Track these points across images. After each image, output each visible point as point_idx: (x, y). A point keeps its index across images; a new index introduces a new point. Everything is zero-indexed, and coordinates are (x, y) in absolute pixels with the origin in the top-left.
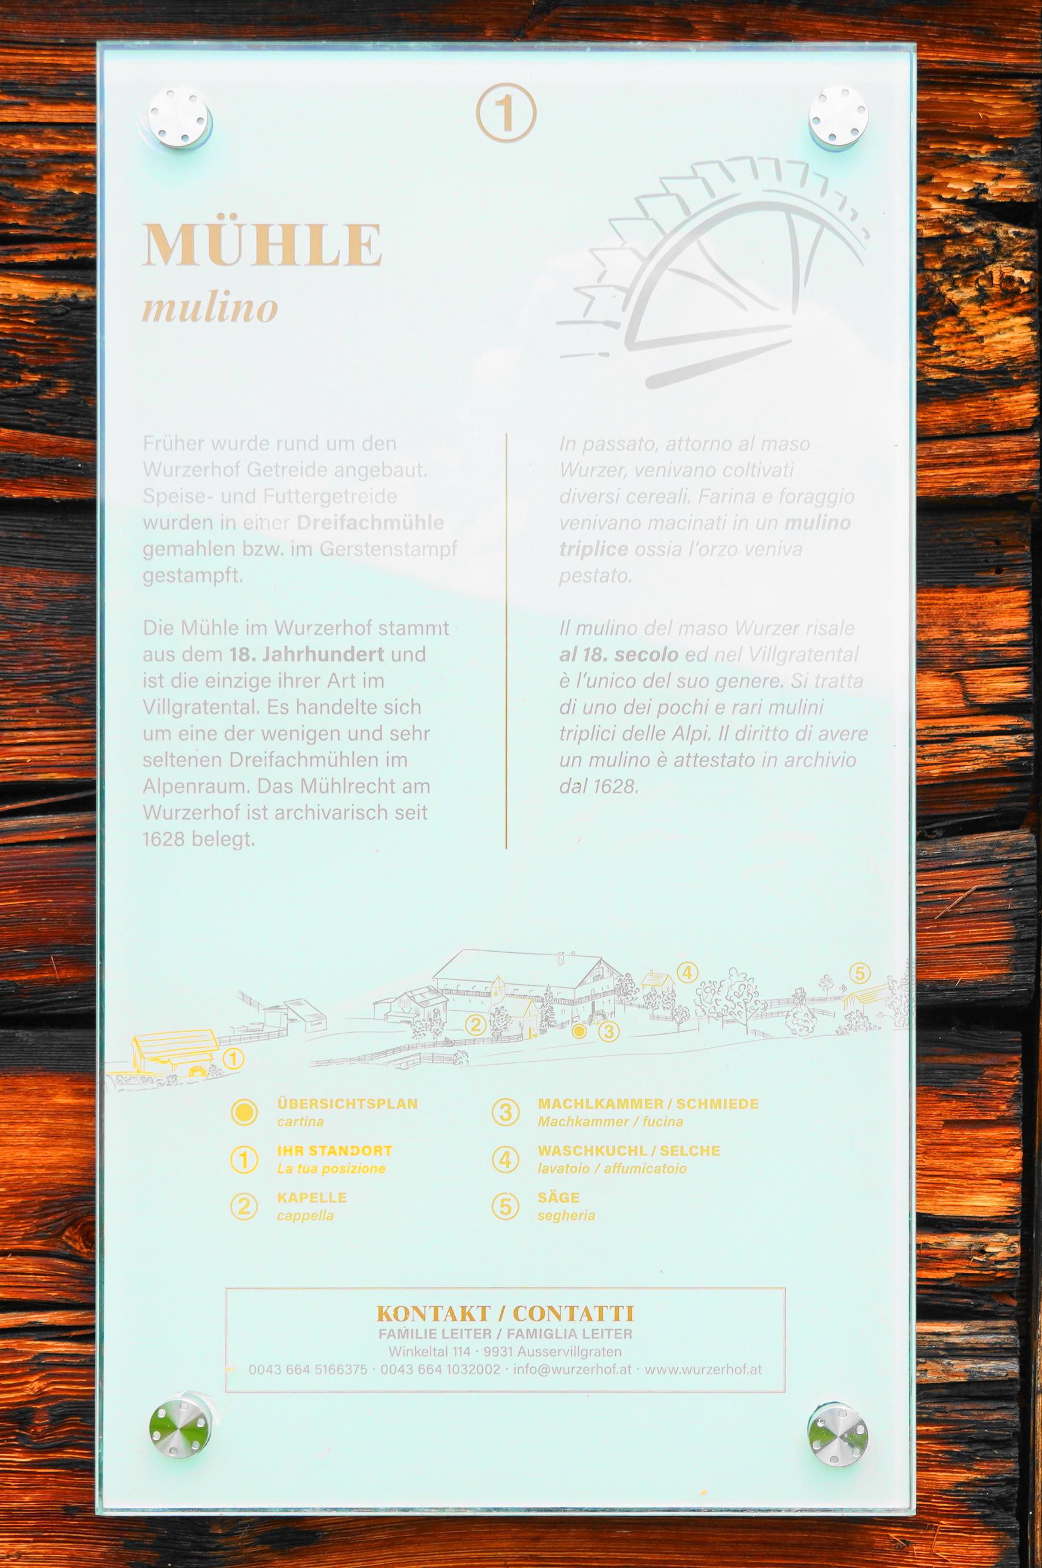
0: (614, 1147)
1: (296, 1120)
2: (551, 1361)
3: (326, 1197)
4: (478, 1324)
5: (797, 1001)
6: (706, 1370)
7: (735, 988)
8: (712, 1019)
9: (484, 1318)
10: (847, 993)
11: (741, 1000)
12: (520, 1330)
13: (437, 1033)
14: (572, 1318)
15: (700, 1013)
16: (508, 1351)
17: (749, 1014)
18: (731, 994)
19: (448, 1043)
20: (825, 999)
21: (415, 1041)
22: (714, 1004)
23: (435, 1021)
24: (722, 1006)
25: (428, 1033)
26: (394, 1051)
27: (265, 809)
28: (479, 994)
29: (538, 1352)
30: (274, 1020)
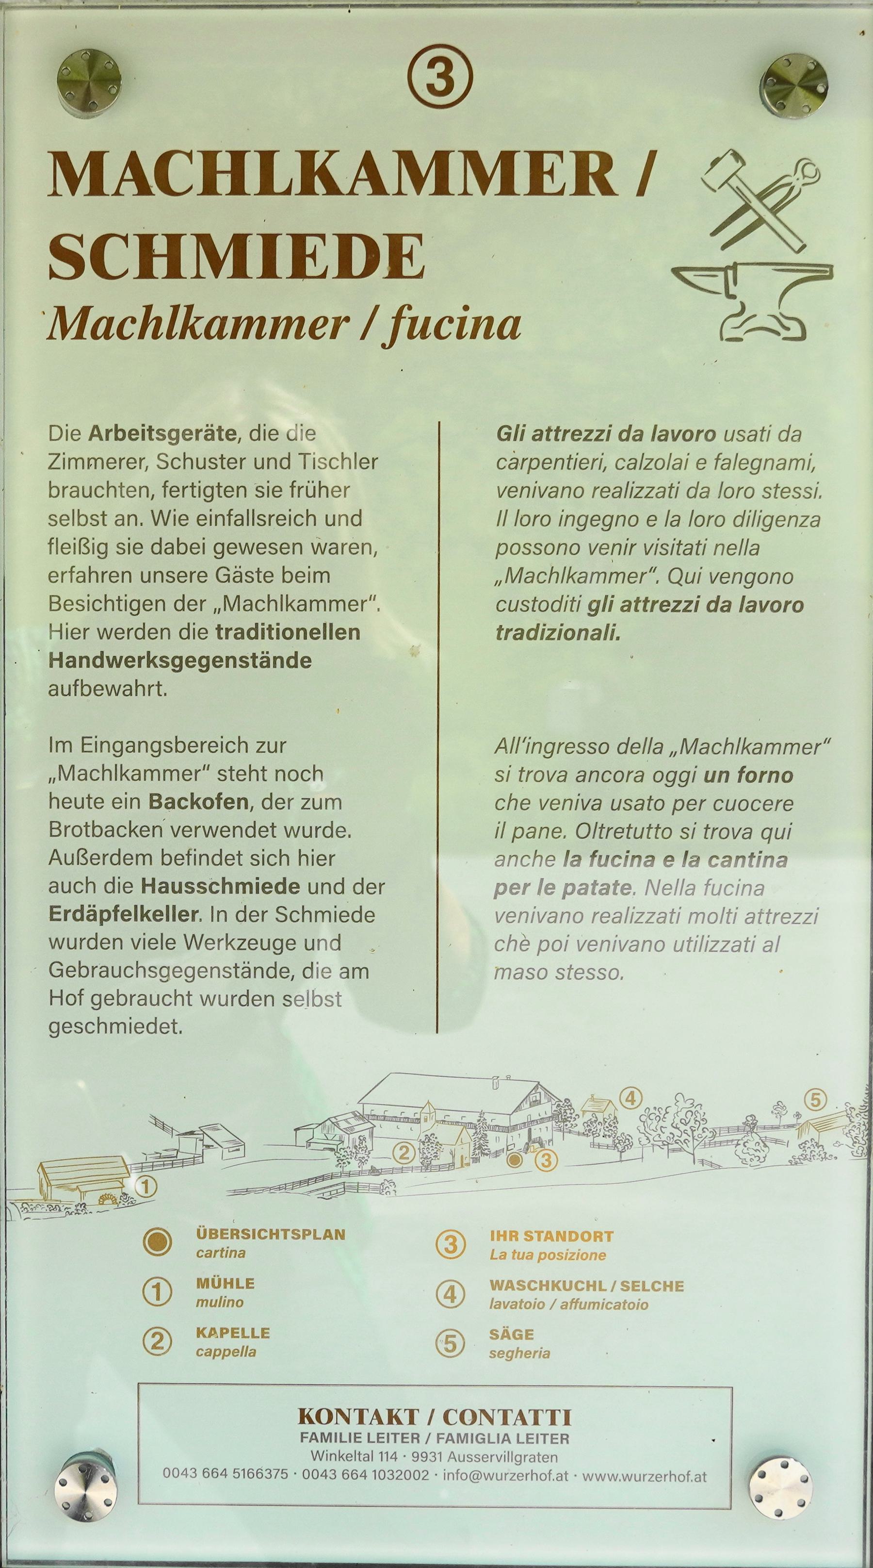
0: (571, 1282)
1: (216, 1251)
2: (486, 1468)
3: (248, 1333)
4: (406, 1428)
5: (748, 1129)
6: (647, 1477)
7: (682, 1115)
8: (656, 1148)
9: (412, 1422)
11: (687, 1127)
12: (450, 1434)
13: (362, 1161)
14: (505, 1422)
15: (644, 1141)
16: (438, 1456)
17: (696, 1143)
18: (677, 1120)
19: (374, 1171)
20: (778, 1128)
21: (339, 1170)
22: (659, 1132)
24: (667, 1134)
25: (353, 1161)
26: (316, 1179)
27: (104, 515)
28: (407, 1120)
29: (469, 1458)
30: (189, 1146)
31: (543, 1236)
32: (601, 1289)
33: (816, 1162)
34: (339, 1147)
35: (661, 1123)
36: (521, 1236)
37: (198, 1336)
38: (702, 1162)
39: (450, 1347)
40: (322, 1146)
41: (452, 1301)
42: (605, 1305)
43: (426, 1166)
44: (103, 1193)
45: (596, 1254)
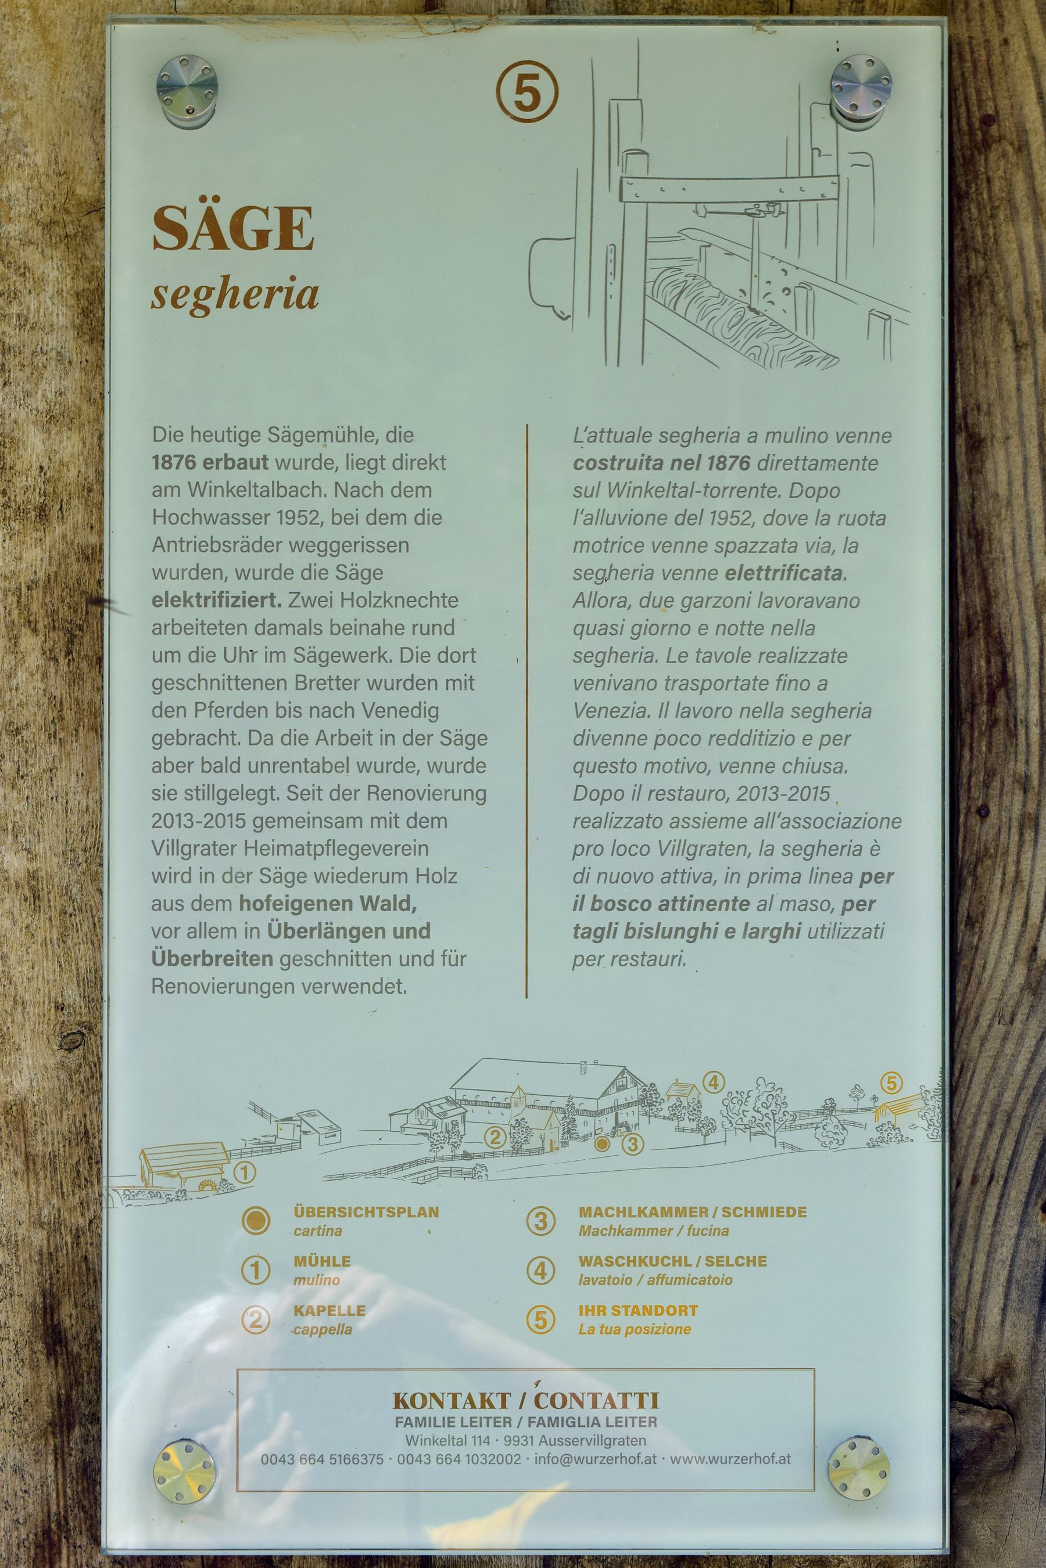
0: (657, 1258)
2: (575, 1451)
4: (498, 1412)
7: (763, 1099)
9: (504, 1406)
10: (878, 1104)
11: (769, 1111)
12: (541, 1418)
15: (727, 1125)
16: (529, 1440)
17: (777, 1126)
18: (759, 1104)
19: (467, 1156)
20: (855, 1111)
22: (741, 1116)
23: (453, 1134)
25: (445, 1146)
26: (411, 1164)
28: (498, 1105)
29: (560, 1442)
30: (287, 1132)
31: (630, 1310)
32: (686, 1265)
33: (893, 1145)
34: (433, 1131)
35: (743, 1107)
36: (609, 1311)
37: (296, 1314)
39: (527, 99)
40: (416, 1132)
41: (543, 1278)
42: (690, 1281)
43: (517, 1151)
44: (204, 1178)
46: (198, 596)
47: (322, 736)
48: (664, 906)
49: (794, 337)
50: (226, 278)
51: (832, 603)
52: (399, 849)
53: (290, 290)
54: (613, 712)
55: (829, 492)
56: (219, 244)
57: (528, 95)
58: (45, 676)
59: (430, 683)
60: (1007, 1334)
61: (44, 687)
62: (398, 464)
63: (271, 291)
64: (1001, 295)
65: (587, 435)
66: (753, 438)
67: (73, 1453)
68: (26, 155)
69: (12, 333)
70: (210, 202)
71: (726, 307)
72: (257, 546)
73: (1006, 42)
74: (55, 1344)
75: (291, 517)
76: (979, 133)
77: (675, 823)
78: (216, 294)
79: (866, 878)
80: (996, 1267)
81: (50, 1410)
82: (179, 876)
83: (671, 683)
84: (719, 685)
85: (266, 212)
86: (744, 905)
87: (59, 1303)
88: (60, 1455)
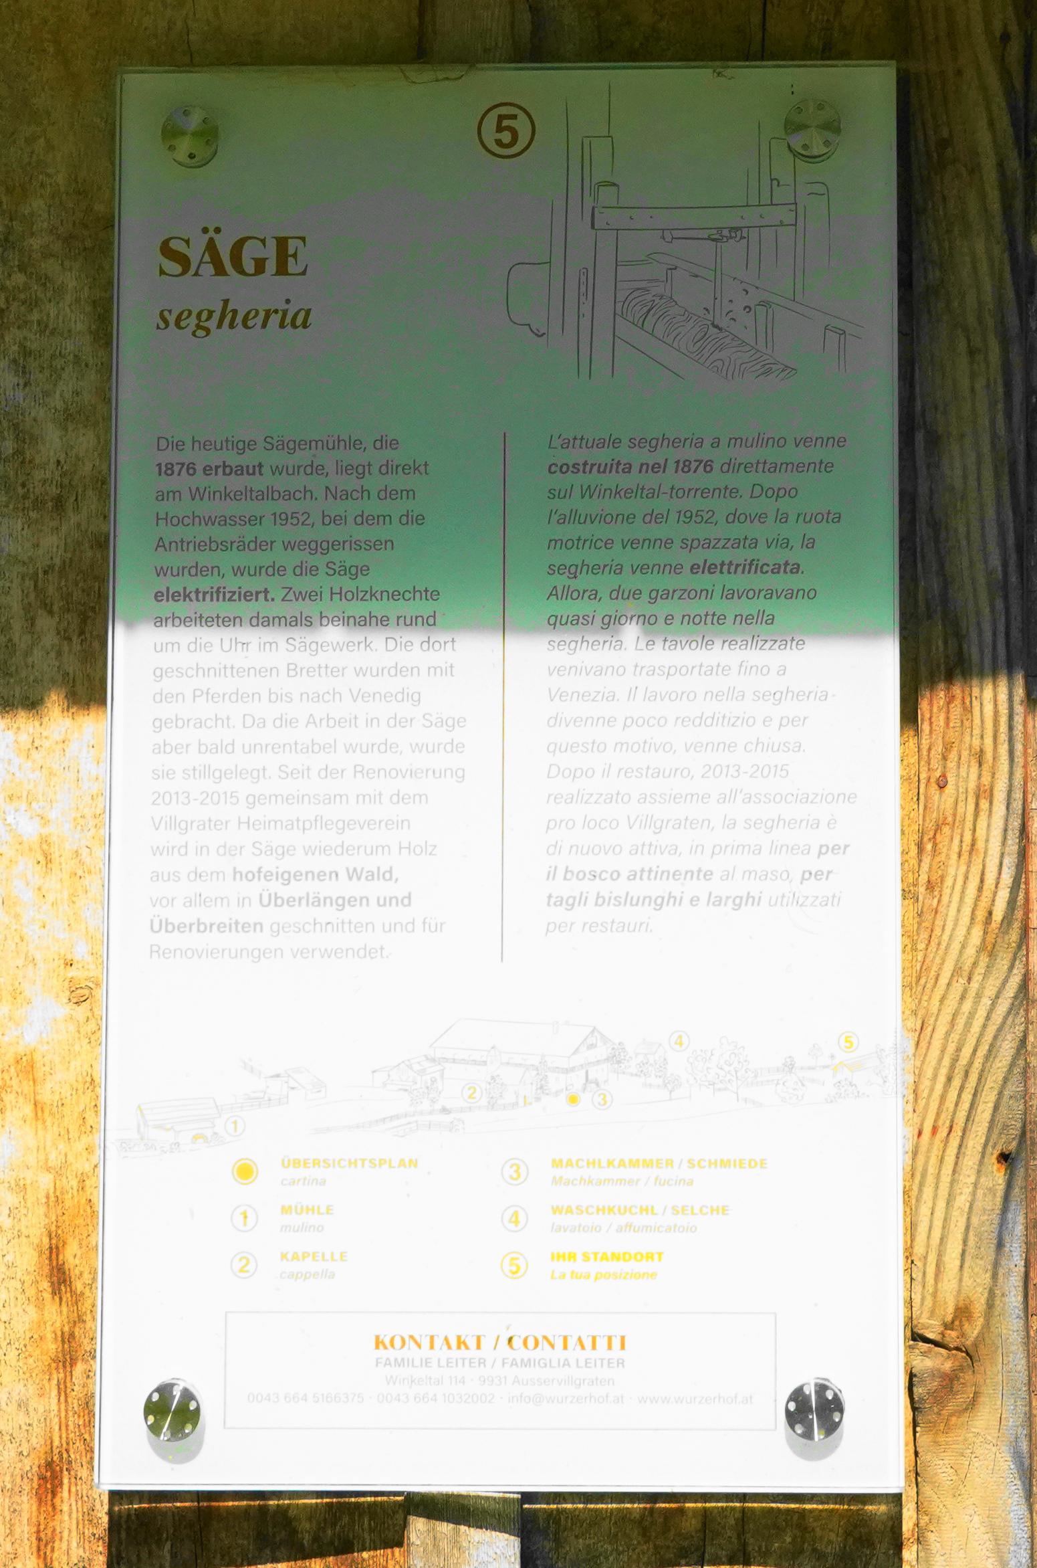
9: (478, 1347)
13: (433, 1101)
19: (445, 1110)
28: (475, 1062)
31: (599, 1256)
38: (745, 1100)
39: (506, 137)
43: (492, 1106)
45: (648, 465)
46: (197, 592)
47: (311, 720)
48: (633, 876)
49: (753, 352)
50: (226, 302)
51: (791, 594)
52: (383, 824)
53: (285, 313)
54: (582, 696)
55: (787, 493)
56: (220, 270)
57: (506, 133)
58: (59, 654)
59: (413, 670)
60: (966, 1279)
61: (57, 664)
62: (384, 469)
63: (268, 314)
64: (956, 304)
65: (560, 441)
66: (716, 443)
67: (76, 1388)
68: (48, 175)
69: (33, 337)
70: (211, 233)
71: (691, 323)
72: (252, 545)
73: (959, 73)
74: (60, 1284)
75: (283, 519)
76: (935, 155)
77: (643, 799)
78: (216, 316)
79: (823, 850)
80: (955, 1213)
81: (54, 1346)
82: (176, 850)
83: (638, 669)
84: (684, 671)
85: (263, 241)
86: (708, 875)
87: (65, 1243)
88: (63, 1390)
